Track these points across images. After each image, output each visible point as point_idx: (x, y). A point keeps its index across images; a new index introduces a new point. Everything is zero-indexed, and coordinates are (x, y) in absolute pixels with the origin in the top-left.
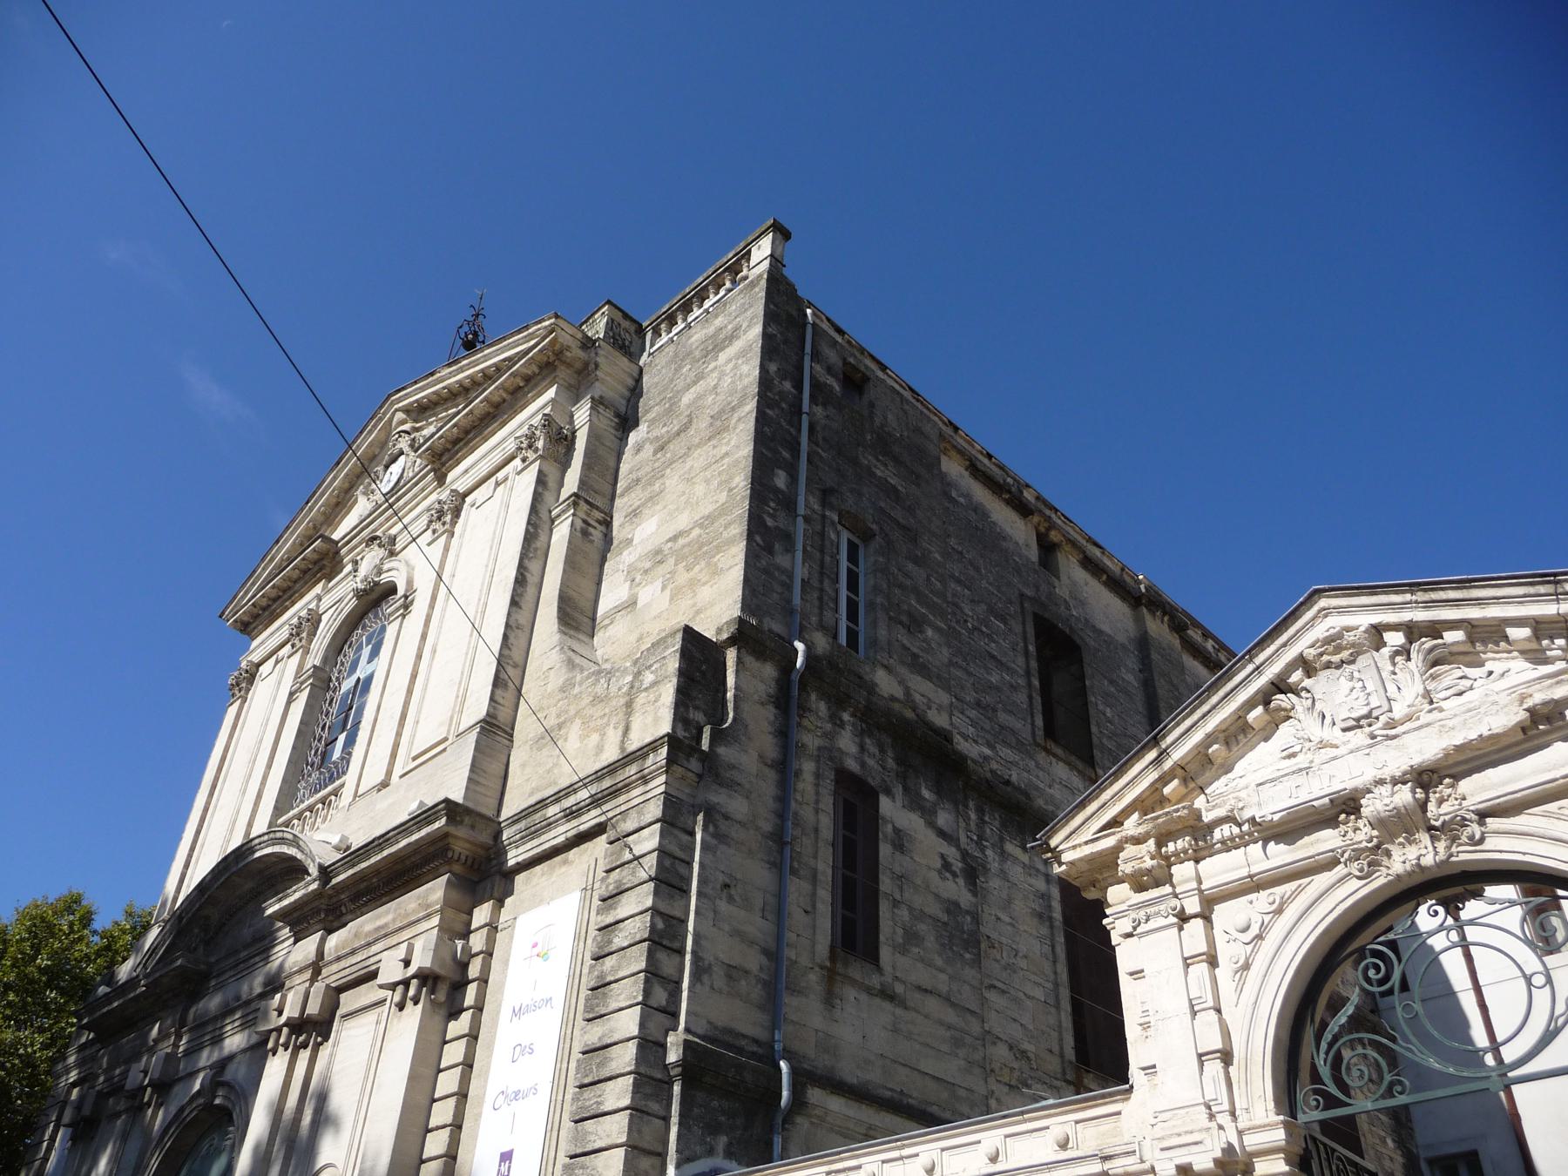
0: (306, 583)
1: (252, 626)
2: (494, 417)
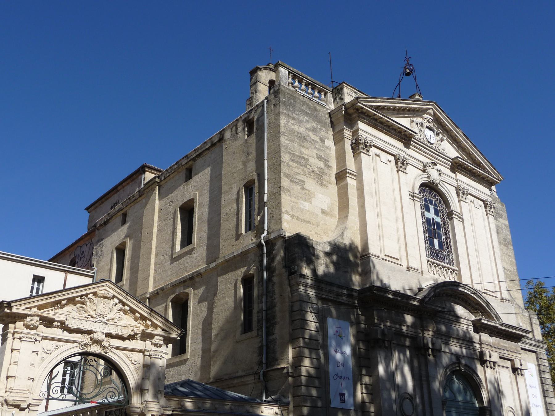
0: (396, 135)
1: (364, 117)
2: (474, 176)
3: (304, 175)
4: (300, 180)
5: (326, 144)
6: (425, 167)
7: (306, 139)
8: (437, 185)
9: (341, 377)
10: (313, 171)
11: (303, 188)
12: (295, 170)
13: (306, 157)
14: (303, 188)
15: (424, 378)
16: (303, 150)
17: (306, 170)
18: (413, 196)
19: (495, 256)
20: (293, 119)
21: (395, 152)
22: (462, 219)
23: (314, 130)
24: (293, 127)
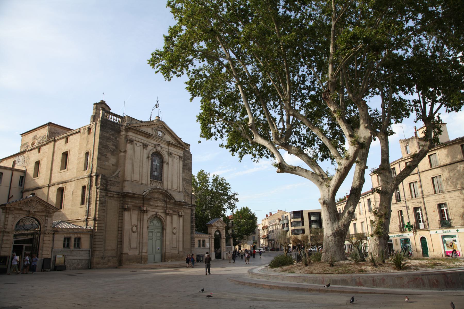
10: (110, 150)
11: (106, 157)
14: (106, 157)
15: (142, 220)
16: (108, 143)
20: (105, 131)
21: (143, 142)
23: (113, 135)
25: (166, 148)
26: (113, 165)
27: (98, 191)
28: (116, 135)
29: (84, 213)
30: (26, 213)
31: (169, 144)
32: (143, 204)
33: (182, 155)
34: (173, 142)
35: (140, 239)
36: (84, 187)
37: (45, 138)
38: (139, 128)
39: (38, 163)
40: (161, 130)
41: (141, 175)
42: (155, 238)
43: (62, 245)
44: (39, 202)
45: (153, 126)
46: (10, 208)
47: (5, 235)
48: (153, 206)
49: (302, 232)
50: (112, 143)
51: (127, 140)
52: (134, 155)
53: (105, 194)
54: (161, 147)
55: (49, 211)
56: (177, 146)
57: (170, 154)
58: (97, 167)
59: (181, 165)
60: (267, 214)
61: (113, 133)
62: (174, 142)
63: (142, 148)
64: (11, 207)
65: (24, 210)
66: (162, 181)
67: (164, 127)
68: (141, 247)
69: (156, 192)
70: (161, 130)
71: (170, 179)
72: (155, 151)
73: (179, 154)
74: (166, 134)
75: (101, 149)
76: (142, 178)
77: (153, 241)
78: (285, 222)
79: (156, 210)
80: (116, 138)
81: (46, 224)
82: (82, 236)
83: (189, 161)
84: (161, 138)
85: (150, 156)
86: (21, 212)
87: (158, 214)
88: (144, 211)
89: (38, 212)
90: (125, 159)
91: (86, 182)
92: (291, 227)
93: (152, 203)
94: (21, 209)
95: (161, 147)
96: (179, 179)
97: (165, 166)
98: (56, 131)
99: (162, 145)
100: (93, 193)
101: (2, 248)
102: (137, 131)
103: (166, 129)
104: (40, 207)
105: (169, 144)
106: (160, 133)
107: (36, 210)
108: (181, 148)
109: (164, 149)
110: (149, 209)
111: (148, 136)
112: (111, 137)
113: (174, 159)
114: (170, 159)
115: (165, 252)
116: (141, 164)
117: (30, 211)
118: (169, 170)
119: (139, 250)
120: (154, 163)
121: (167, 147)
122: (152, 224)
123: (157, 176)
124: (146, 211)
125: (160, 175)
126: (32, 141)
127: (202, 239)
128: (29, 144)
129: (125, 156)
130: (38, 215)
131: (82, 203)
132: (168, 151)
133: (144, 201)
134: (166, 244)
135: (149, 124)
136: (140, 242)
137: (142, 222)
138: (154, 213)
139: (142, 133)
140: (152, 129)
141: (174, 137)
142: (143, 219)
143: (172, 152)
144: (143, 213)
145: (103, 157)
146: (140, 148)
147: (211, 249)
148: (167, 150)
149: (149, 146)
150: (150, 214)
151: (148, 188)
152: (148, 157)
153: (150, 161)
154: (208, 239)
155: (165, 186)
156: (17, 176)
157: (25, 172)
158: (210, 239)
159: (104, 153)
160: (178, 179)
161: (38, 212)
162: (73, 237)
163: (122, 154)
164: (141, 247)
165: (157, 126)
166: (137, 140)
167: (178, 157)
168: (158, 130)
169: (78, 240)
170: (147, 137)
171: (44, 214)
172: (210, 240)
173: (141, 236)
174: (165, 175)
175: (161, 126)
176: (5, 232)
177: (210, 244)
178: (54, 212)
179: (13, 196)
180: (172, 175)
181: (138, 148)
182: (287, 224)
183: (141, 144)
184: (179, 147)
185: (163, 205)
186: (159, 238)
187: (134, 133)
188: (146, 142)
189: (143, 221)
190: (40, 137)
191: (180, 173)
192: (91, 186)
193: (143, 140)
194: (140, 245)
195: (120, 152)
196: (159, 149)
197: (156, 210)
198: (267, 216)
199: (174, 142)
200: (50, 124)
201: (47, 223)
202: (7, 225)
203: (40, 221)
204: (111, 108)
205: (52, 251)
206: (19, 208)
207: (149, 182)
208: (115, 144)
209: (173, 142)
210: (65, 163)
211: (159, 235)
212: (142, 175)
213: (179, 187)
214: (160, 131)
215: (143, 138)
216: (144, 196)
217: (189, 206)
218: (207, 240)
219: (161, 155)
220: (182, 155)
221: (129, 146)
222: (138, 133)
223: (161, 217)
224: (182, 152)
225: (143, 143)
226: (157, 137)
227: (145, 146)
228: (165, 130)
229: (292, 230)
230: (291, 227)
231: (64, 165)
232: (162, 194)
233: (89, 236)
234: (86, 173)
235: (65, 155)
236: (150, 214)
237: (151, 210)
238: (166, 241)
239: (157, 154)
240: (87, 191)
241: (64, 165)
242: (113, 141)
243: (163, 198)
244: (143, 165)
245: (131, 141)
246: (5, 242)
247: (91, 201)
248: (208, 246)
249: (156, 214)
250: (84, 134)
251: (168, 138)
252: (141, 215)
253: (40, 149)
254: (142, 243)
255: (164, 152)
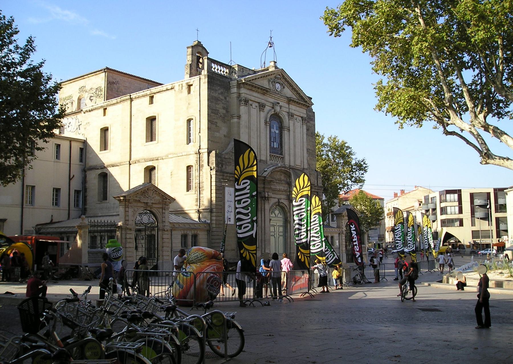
3: (217, 119)
4: (216, 122)
5: (227, 100)
6: (273, 105)
7: (218, 100)
8: (279, 114)
9: (392, 75)
10: (221, 116)
11: (216, 126)
12: (214, 117)
13: (218, 109)
14: (216, 126)
15: (263, 210)
16: (217, 106)
17: (218, 116)
18: (266, 123)
19: (303, 146)
20: (213, 90)
21: (259, 100)
22: (289, 130)
23: (222, 93)
24: (213, 94)
25: (285, 107)
26: (225, 136)
27: (212, 174)
28: (226, 94)
29: (194, 203)
30: (143, 205)
31: (290, 101)
32: (264, 188)
33: (305, 116)
34: (294, 97)
35: (262, 235)
36: (189, 168)
37: (101, 91)
38: (253, 81)
39: (105, 131)
40: (279, 81)
41: (302, 162)
42: (277, 234)
43: (180, 245)
44: (155, 190)
45: (269, 77)
46: (129, 199)
47: (128, 232)
48: (274, 191)
49: (458, 223)
50: (222, 105)
51: (240, 101)
52: (249, 121)
53: (221, 177)
54: (281, 107)
55: (166, 202)
56: (300, 103)
57: (291, 115)
58: (208, 140)
59: (305, 131)
60: (396, 192)
61: (222, 90)
62: (295, 97)
63: (258, 110)
64: (131, 198)
65: (142, 202)
66: (282, 155)
67: (283, 76)
68: (263, 246)
69: (278, 171)
70: (279, 81)
71: (292, 152)
72: (273, 113)
73: (302, 115)
74: (286, 87)
75: (211, 116)
76: (260, 152)
77: (275, 237)
78: (431, 206)
79: (278, 196)
80: (225, 98)
81: (164, 218)
82: (199, 232)
83: (311, 122)
84: (279, 93)
85: (268, 120)
86: (139, 204)
87: (280, 201)
88: (265, 197)
89: (155, 203)
90: (239, 127)
91: (192, 161)
92: (441, 214)
93: (273, 187)
94: (139, 201)
95: (281, 107)
96: (303, 150)
97: (285, 133)
98: (115, 79)
99: (281, 104)
100: (204, 175)
101: (126, 248)
102: (253, 86)
103: (286, 79)
104: (158, 198)
105: (290, 101)
106: (278, 86)
107: (154, 202)
108: (304, 105)
109: (283, 109)
110: (271, 194)
111: (265, 91)
112: (220, 98)
113: (296, 122)
114: (291, 123)
115: (290, 253)
116: (259, 133)
117: (147, 203)
118: (291, 138)
119: (262, 250)
120: (272, 130)
121: (287, 106)
122: (273, 215)
123: (276, 148)
124: (268, 197)
125: (280, 147)
126: (79, 95)
127: (330, 235)
128: (73, 99)
129: (239, 123)
130: (155, 207)
131: (188, 188)
132: (288, 111)
133: (264, 184)
134: (290, 242)
135: (266, 75)
136: (262, 240)
137: (263, 212)
138: (276, 200)
139: (258, 88)
140: (269, 81)
141: (295, 91)
142: (264, 209)
143: (293, 112)
144: (264, 200)
145: (214, 126)
146: (299, 124)
147: (341, 248)
148: (287, 110)
149: (266, 106)
150: (273, 201)
151: (269, 165)
152: (266, 123)
153: (268, 127)
154: (337, 235)
155: (287, 163)
156: (76, 148)
157: (85, 142)
158: (339, 234)
159: (215, 121)
160: (302, 151)
161: (155, 203)
162: (190, 233)
163: (235, 120)
164: (263, 246)
165: (273, 76)
166: (253, 98)
167: (300, 118)
168: (276, 81)
169: (195, 237)
170: (264, 94)
171: (161, 206)
172: (339, 236)
173: (263, 232)
174: (286, 147)
175: (280, 75)
176: (128, 229)
177: (339, 242)
178: (170, 203)
179: (74, 176)
180: (295, 146)
181: (254, 111)
182: (434, 209)
183: (257, 104)
184: (302, 104)
185: (286, 188)
186: (282, 234)
187: (248, 89)
188: (263, 101)
189: (264, 211)
190: (91, 89)
191: (303, 143)
192: (200, 166)
193: (259, 98)
194: (262, 244)
195: (232, 117)
196: (278, 109)
197: (278, 196)
198: (396, 195)
199: (295, 97)
200: (108, 70)
201: (165, 217)
202: (128, 220)
203: (157, 215)
204: (209, 52)
205: (171, 252)
206: (137, 199)
207: (268, 158)
208: (225, 106)
209: (294, 97)
210: (150, 131)
211: (281, 229)
212: (260, 149)
213: (304, 163)
214: (279, 83)
215: (259, 95)
216: (265, 177)
217: (315, 189)
218: (336, 236)
219: (280, 117)
220: (305, 116)
221: (243, 109)
222: (254, 89)
223: (284, 206)
224: (305, 112)
225: (259, 103)
226: (276, 92)
227: (262, 106)
228: (283, 80)
229: (441, 220)
230: (441, 214)
231: (151, 135)
232: (285, 173)
233: (206, 233)
234: (193, 148)
235: (151, 120)
236: (273, 201)
237: (273, 196)
238: (290, 238)
239: (276, 117)
240: (194, 173)
241: (151, 135)
242: (222, 103)
243: (285, 179)
244: (261, 134)
245: (246, 101)
246: (128, 240)
247: (203, 187)
248: (338, 244)
249: (279, 202)
250: (181, 92)
251: (288, 92)
252: (261, 203)
253: (105, 109)
254: (265, 241)
255: (284, 113)
